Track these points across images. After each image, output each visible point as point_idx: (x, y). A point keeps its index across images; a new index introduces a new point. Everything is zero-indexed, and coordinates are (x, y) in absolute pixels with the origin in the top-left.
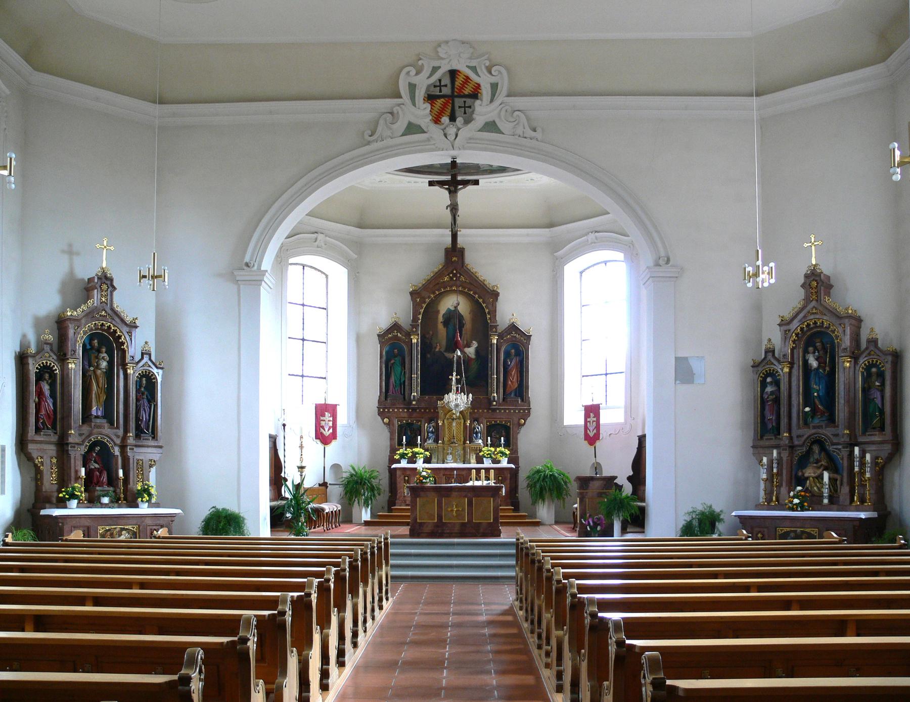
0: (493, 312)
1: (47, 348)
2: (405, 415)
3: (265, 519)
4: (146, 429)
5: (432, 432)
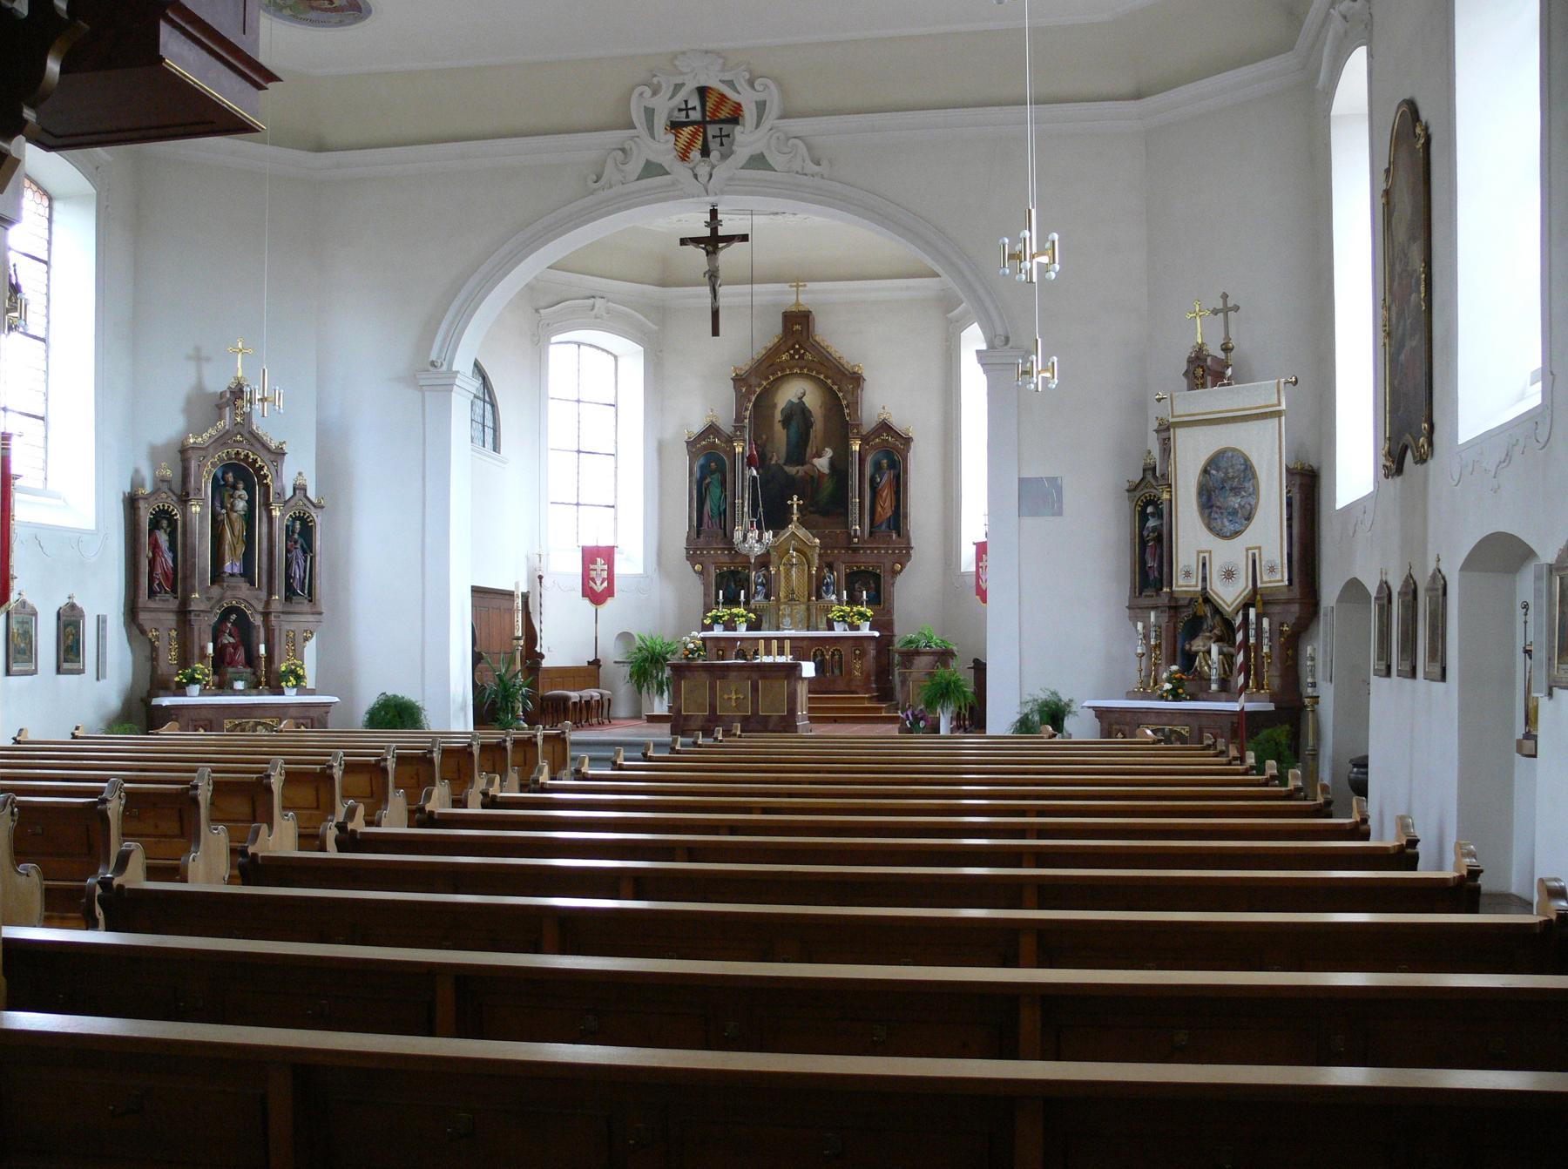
0: (855, 405)
1: (164, 487)
2: (727, 559)
3: (464, 708)
4: (301, 591)
5: (762, 584)
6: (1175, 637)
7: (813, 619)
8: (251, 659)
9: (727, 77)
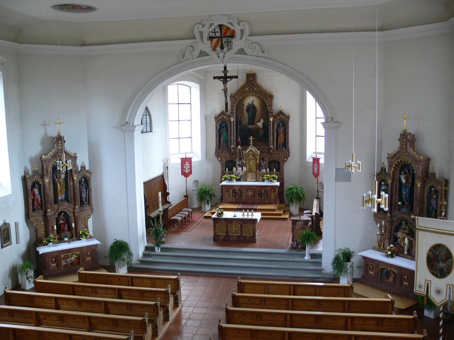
0: (271, 105)
2: (229, 156)
3: (143, 238)
6: (391, 231)
7: (258, 178)
8: (70, 228)
9: (230, 21)
